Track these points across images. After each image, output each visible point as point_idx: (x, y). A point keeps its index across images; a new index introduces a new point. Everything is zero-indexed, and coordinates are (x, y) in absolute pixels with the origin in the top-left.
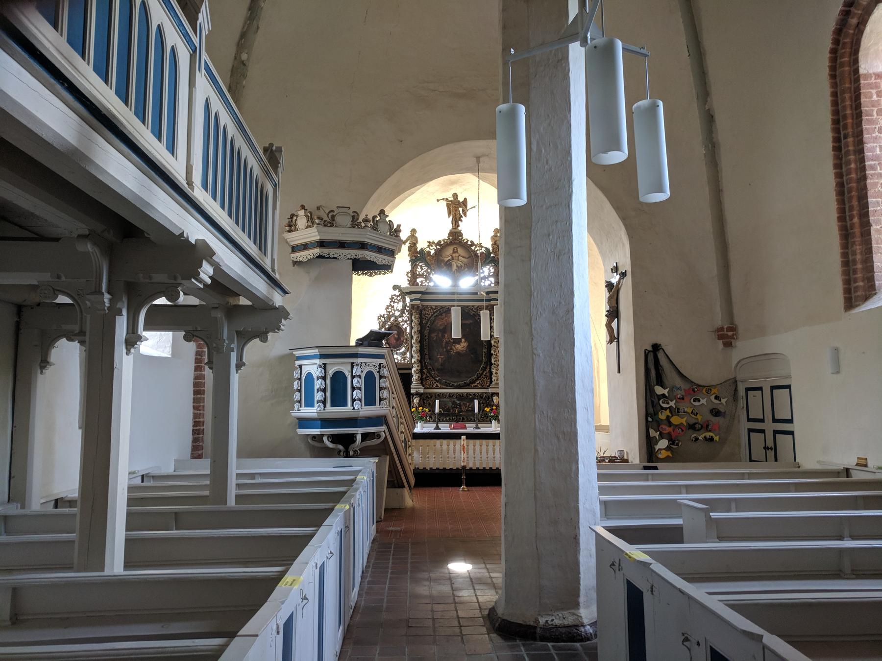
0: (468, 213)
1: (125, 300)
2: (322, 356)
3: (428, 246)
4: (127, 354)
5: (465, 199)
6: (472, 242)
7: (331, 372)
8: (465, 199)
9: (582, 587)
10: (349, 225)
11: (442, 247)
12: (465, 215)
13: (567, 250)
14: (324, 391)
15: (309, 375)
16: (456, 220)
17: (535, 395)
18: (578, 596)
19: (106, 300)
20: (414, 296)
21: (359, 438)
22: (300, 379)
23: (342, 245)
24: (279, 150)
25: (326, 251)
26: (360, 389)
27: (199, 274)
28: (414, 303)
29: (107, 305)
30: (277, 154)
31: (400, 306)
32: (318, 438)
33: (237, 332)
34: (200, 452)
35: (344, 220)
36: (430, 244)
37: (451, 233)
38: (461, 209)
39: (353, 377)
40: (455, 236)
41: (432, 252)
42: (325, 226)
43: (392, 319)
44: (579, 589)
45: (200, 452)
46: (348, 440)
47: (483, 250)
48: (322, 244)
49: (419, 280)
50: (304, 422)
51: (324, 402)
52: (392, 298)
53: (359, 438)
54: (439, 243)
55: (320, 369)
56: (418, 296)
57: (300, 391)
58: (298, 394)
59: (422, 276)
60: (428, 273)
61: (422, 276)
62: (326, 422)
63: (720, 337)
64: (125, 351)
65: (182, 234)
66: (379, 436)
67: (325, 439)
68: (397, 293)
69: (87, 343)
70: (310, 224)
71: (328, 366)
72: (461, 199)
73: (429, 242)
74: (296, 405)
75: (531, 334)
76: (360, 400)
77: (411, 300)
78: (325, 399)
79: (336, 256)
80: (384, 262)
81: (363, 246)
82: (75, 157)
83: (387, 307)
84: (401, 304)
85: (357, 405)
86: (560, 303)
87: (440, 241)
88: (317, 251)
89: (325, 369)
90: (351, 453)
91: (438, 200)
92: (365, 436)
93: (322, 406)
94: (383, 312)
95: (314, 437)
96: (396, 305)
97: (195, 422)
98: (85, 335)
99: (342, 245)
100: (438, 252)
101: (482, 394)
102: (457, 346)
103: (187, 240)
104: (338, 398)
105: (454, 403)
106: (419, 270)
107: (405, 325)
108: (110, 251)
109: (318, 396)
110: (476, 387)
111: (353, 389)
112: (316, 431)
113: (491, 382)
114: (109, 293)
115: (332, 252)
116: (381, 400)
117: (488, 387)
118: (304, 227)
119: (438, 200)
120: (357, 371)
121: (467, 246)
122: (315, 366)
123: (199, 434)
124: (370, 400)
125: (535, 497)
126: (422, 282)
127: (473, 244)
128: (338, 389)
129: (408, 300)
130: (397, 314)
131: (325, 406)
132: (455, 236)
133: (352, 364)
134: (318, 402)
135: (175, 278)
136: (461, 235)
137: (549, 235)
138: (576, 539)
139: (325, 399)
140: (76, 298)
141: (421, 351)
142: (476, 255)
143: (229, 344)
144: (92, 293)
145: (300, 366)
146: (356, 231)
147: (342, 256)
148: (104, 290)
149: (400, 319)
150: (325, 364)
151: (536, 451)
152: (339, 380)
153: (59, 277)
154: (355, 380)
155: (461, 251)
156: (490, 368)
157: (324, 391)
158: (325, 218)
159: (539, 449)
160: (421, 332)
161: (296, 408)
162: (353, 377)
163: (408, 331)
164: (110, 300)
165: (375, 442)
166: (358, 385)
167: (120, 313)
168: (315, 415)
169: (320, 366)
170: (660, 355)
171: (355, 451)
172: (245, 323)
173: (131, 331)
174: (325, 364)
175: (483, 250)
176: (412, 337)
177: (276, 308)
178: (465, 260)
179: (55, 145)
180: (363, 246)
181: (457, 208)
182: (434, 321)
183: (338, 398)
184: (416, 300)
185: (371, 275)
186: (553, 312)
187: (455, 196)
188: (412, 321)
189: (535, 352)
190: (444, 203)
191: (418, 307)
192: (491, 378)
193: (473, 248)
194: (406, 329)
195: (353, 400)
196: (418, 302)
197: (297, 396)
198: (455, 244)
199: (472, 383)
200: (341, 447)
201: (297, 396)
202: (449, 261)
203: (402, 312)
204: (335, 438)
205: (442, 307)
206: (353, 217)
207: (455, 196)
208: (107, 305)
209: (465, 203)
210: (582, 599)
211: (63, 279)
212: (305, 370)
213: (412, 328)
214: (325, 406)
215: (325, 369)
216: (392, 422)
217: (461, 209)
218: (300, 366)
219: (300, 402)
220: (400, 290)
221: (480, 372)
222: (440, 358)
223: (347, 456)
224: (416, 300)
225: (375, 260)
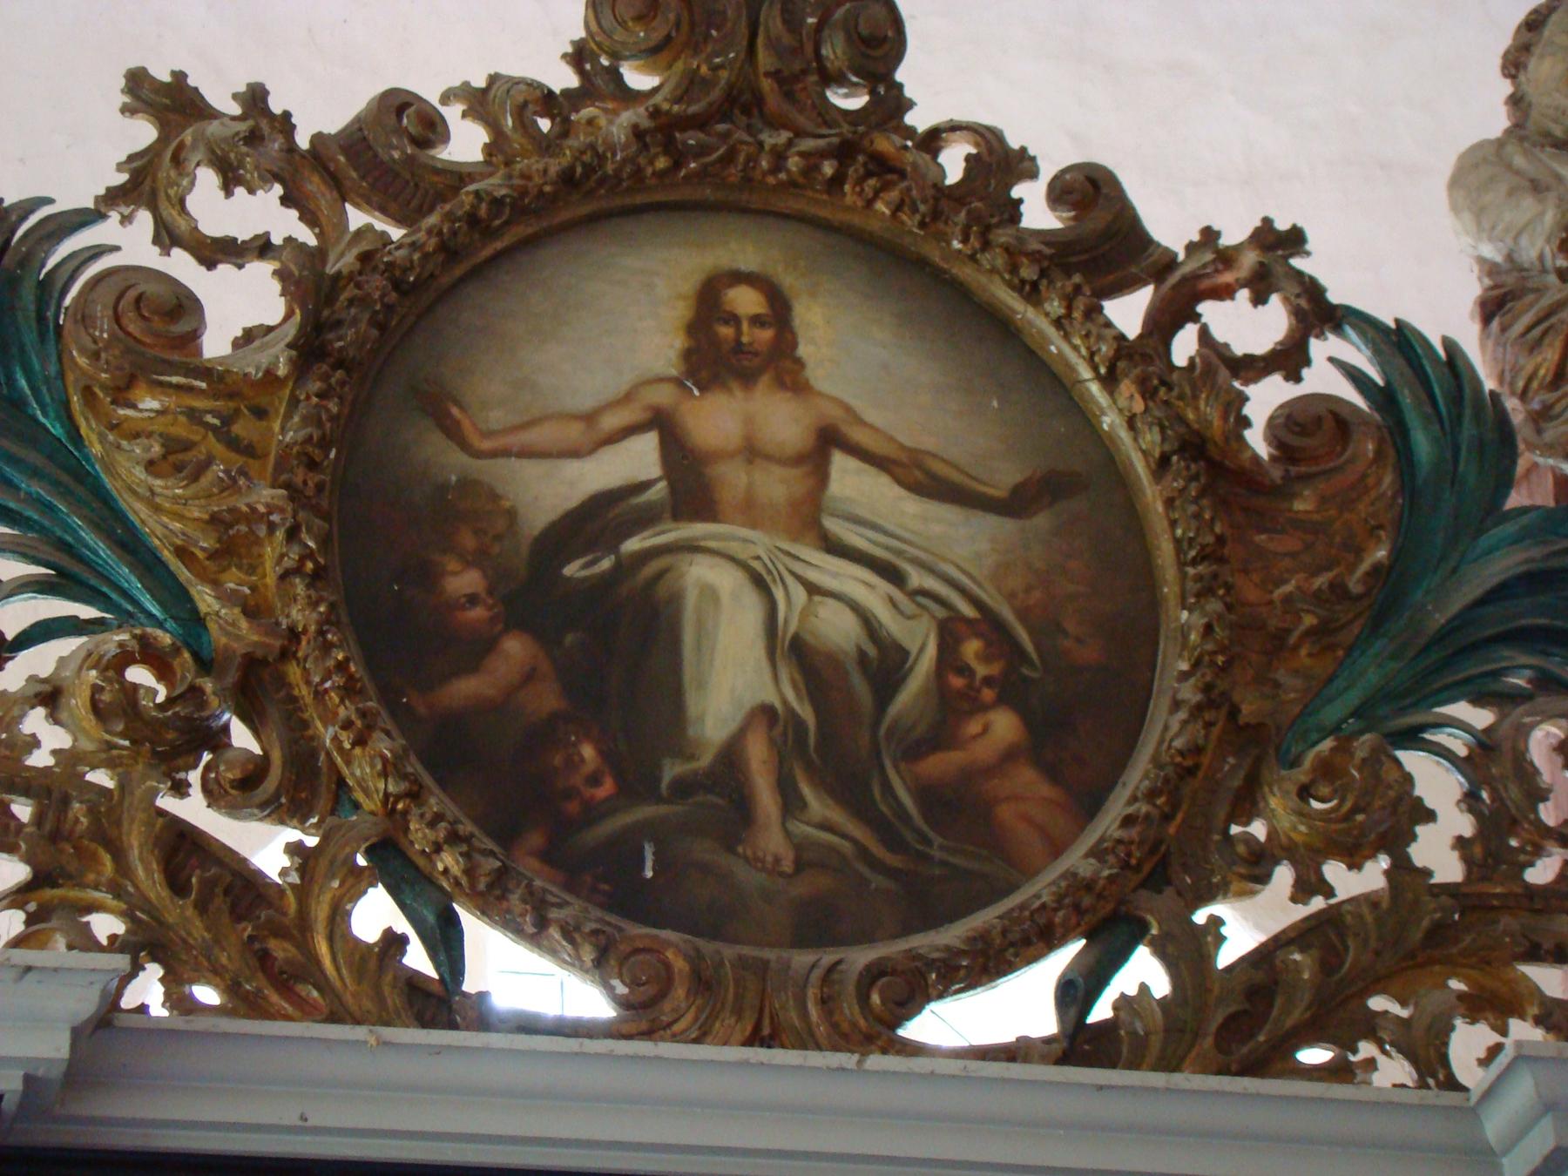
3: (144, 185)
41: (240, 307)
73: (168, 101)
87: (403, 119)
127: (1103, 233)
142: (1205, 456)
155: (854, 351)
178: (963, 544)
198: (729, 196)
202: (600, 518)
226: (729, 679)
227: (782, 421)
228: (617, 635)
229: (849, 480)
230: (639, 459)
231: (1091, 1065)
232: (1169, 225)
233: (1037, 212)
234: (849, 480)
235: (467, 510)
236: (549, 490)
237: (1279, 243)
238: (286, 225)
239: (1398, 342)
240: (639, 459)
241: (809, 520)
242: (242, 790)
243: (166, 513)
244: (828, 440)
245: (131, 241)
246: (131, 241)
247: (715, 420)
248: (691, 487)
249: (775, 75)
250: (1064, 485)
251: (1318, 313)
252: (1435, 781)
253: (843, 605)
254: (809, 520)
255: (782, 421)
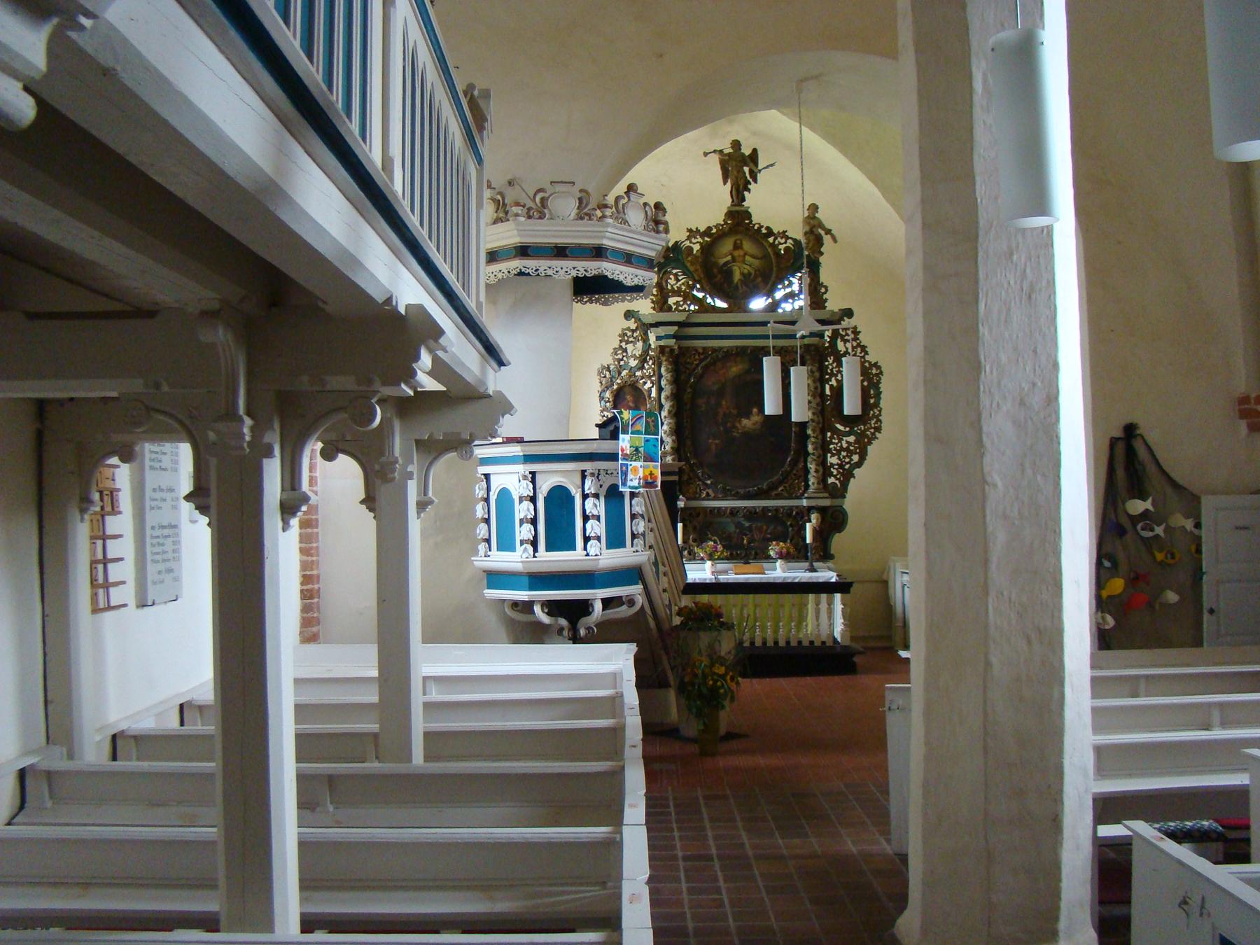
0: (759, 176)
1: (277, 426)
2: (528, 459)
3: (689, 238)
4: (284, 530)
5: (755, 151)
6: (768, 228)
7: (545, 486)
8: (755, 151)
9: (1063, 905)
10: (573, 215)
11: (713, 238)
12: (756, 181)
13: (1044, 283)
14: (534, 522)
15: (504, 493)
16: (739, 192)
17: (986, 562)
18: (1057, 918)
19: (246, 430)
20: (662, 331)
21: (598, 606)
22: (487, 500)
23: (560, 252)
24: (486, 94)
25: (530, 264)
26: (598, 518)
27: (414, 373)
28: (662, 343)
29: (248, 438)
30: (482, 103)
31: (636, 349)
32: (527, 606)
33: (417, 442)
34: (314, 629)
35: (566, 206)
36: (692, 233)
37: (730, 214)
38: (746, 169)
39: (585, 497)
40: (738, 219)
41: (696, 248)
42: (529, 217)
43: (624, 373)
44: (1058, 908)
45: (314, 629)
46: (574, 611)
47: (790, 243)
48: (523, 251)
49: (672, 301)
50: (496, 578)
51: (534, 543)
52: (623, 335)
53: (598, 606)
54: (707, 232)
55: (524, 483)
56: (672, 330)
57: (487, 521)
58: (483, 526)
59: (677, 293)
60: (688, 286)
61: (677, 293)
62: (539, 579)
63: (1244, 414)
64: (280, 524)
65: (389, 300)
66: (631, 602)
67: (537, 609)
68: (632, 324)
69: (213, 510)
70: (502, 215)
71: (538, 477)
72: (747, 151)
73: (690, 231)
74: (482, 547)
75: (980, 442)
76: (599, 539)
77: (658, 338)
78: (535, 537)
79: (550, 272)
80: (636, 282)
81: (598, 252)
82: (262, 199)
83: (615, 352)
84: (640, 344)
85: (593, 547)
86: (1034, 384)
87: (709, 228)
88: (516, 264)
89: (533, 481)
90: (582, 632)
91: (706, 154)
92: (607, 603)
93: (531, 549)
94: (609, 360)
95: (515, 604)
96: (630, 347)
97: (304, 576)
98: (208, 496)
99: (560, 252)
100: (707, 250)
101: (791, 508)
102: (745, 422)
103: (395, 311)
104: (560, 536)
105: (738, 525)
106: (672, 281)
107: (649, 385)
108: (252, 334)
109: (525, 532)
110: (778, 497)
111: (586, 518)
112: (522, 595)
113: (807, 486)
114: (249, 414)
115: (543, 265)
116: (634, 536)
117: (800, 497)
118: (490, 220)
119: (706, 154)
120: (590, 486)
121: (761, 236)
122: (516, 477)
123: (311, 597)
124: (615, 539)
125: (986, 750)
126: (677, 303)
127: (770, 232)
128: (558, 517)
129: (652, 337)
130: (633, 363)
131: (535, 550)
132: (738, 219)
133: (583, 472)
134: (522, 542)
135: (370, 382)
136: (749, 215)
137: (1011, 254)
138: (1056, 822)
139: (535, 537)
140: (187, 422)
141: (677, 431)
142: (777, 253)
143: (405, 466)
144: (220, 418)
145: (487, 476)
146: (585, 226)
147: (562, 272)
148: (241, 411)
149: (639, 373)
150: (533, 474)
151: (988, 664)
152: (559, 501)
153: (157, 386)
154: (590, 503)
155: (748, 246)
156: (805, 462)
157: (534, 522)
158: (530, 204)
159: (994, 660)
160: (676, 397)
161: (482, 553)
162: (585, 497)
163: (654, 394)
164: (252, 429)
165: (623, 611)
166: (595, 513)
167: (269, 453)
168: (519, 567)
169: (525, 478)
170: (1138, 446)
171: (589, 629)
172: (438, 426)
173: (288, 486)
174: (533, 474)
175: (790, 243)
176: (661, 407)
177: (489, 396)
178: (756, 263)
179: (240, 180)
180: (598, 252)
181: (739, 167)
182: (702, 376)
183: (560, 536)
184: (667, 337)
185: (605, 304)
186: (1022, 403)
187: (736, 145)
188: (660, 376)
189: (989, 479)
190: (715, 159)
191: (672, 350)
192: (806, 481)
193: (771, 240)
194: (650, 390)
195: (586, 539)
196: (672, 342)
197: (482, 530)
198: (737, 233)
199: (773, 487)
200: (563, 622)
201: (482, 530)
202: (726, 264)
203: (643, 360)
204: (554, 608)
205: (714, 350)
206: (580, 200)
207: (736, 145)
208: (248, 438)
209: (754, 156)
210: (1062, 924)
211: (165, 388)
212: (496, 484)
213: (660, 389)
214: (535, 550)
215: (533, 481)
216: (649, 573)
217: (746, 169)
218: (487, 476)
219: (488, 541)
220: (638, 320)
221: (786, 467)
222: (714, 443)
223: (576, 639)
224: (667, 337)
225: (621, 278)
226: (737, 276)
227: (741, 253)
228: (728, 273)
229: (748, 258)
230: (729, 258)
231: (1057, 533)
232: (775, 231)
233: (764, 231)
234: (748, 258)
235: (716, 264)
236: (722, 261)
237: (784, 232)
238: (700, 240)
239: (795, 240)
240: (729, 258)
241: (744, 262)
242: (698, 290)
243: (692, 269)
244: (746, 254)
245: (687, 243)
246: (687, 243)
247: (736, 253)
248: (734, 260)
249: (667, 685)
250: (765, 257)
251: (788, 238)
252: (795, 280)
253: (746, 269)
254: (744, 262)
255: (741, 253)
